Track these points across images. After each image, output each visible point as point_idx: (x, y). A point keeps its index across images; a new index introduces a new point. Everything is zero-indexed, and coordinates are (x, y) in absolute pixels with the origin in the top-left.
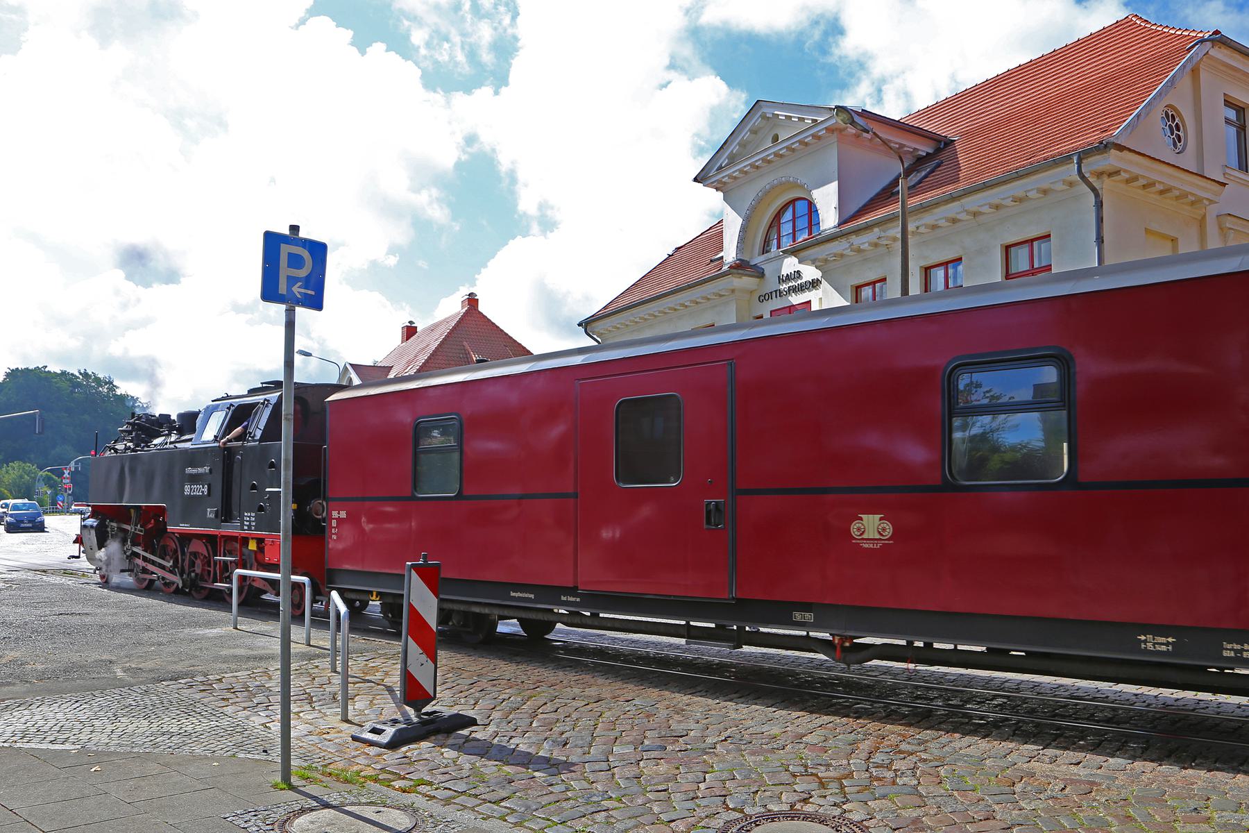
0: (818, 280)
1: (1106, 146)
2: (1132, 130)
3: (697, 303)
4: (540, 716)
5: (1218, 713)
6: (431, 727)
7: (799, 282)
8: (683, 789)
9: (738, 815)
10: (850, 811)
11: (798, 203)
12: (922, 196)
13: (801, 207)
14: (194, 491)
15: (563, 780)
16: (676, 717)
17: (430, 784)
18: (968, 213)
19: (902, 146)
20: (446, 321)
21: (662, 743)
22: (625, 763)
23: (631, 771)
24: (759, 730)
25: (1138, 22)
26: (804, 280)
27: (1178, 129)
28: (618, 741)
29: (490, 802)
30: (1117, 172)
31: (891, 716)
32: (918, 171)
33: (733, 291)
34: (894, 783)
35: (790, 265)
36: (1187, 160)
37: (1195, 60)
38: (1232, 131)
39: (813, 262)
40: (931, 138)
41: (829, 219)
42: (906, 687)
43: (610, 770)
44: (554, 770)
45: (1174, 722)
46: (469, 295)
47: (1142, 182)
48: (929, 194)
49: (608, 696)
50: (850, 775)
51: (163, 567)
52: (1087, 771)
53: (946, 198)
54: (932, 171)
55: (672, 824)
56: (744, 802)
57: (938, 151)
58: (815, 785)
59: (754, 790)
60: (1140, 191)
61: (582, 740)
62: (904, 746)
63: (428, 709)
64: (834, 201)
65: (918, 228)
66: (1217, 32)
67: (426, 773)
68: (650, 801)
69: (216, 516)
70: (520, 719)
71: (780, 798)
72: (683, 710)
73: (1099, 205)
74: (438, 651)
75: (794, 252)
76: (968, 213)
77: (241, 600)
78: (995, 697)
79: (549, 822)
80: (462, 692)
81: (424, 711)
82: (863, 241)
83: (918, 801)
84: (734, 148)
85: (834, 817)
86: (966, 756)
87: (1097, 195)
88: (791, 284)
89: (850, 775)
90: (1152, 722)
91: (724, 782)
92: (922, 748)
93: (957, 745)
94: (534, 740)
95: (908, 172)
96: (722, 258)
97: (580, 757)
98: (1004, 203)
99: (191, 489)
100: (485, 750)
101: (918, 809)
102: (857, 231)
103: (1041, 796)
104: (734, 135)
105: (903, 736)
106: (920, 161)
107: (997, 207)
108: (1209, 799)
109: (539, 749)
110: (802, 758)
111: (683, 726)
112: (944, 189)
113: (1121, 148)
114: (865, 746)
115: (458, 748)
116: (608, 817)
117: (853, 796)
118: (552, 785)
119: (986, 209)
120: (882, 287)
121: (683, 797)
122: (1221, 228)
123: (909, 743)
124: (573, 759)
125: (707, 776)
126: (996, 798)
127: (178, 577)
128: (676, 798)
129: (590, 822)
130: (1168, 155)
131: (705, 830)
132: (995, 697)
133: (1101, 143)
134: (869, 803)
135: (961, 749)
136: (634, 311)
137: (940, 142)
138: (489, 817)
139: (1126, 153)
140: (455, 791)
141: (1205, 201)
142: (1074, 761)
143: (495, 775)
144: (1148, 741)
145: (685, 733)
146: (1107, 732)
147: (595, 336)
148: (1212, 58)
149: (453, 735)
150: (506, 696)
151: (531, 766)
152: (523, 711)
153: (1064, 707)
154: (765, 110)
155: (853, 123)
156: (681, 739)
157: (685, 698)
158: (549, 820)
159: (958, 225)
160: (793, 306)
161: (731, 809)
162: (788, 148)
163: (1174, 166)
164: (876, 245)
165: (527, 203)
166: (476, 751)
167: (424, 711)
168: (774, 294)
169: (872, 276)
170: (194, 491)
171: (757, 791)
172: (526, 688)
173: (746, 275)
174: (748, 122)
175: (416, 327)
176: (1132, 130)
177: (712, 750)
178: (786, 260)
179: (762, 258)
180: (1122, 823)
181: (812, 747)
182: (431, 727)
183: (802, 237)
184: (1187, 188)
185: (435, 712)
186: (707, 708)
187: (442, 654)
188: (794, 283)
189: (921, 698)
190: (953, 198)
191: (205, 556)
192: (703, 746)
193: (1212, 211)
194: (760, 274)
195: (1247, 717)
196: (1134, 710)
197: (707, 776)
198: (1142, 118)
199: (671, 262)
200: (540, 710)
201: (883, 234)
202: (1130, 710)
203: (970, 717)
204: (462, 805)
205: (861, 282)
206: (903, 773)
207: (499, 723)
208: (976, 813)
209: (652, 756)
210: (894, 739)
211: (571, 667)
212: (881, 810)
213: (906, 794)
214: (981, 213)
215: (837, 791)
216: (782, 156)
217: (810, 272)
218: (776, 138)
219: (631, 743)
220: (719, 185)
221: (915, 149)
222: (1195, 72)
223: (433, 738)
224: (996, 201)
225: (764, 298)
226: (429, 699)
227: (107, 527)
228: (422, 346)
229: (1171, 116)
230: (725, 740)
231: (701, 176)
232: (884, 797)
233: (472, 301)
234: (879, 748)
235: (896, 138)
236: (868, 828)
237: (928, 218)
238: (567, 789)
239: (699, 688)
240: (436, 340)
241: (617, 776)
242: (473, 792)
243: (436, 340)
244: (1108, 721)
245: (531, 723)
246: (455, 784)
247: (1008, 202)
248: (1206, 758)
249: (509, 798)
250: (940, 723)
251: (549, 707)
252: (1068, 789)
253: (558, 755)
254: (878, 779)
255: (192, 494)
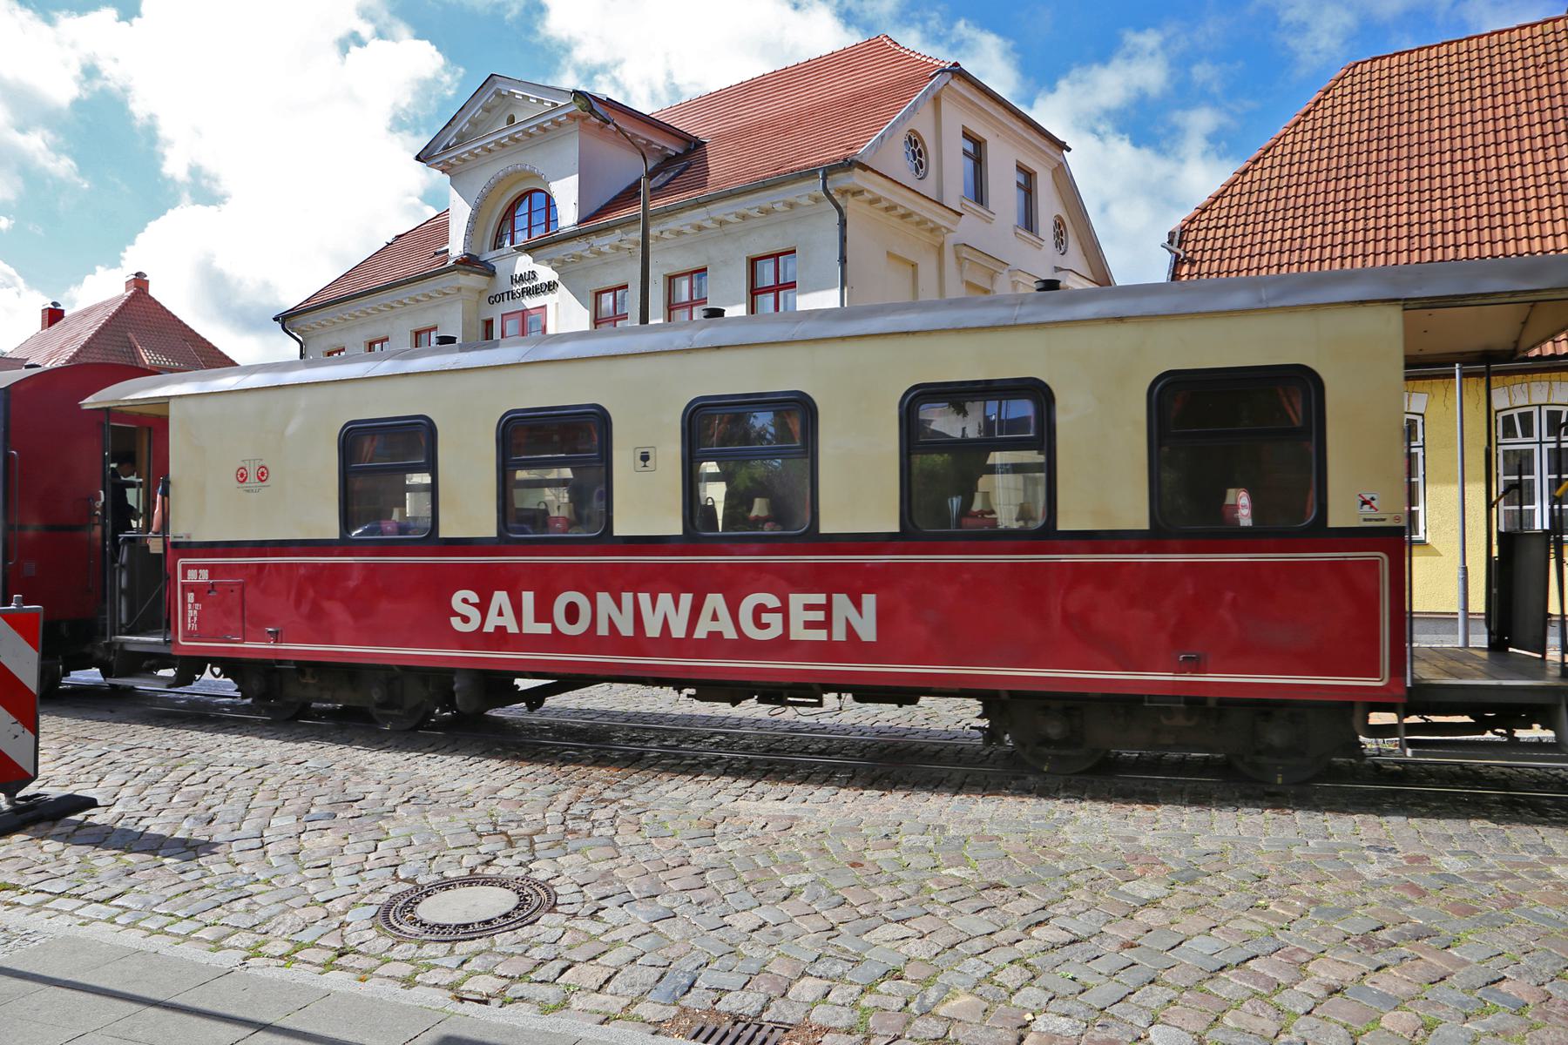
0: (554, 282)
1: (850, 164)
2: (875, 152)
3: (417, 301)
4: (184, 790)
5: (926, 738)
6: (30, 814)
7: (534, 283)
8: (348, 862)
9: (408, 886)
10: (537, 870)
11: (536, 196)
12: (668, 199)
13: (539, 200)
15: (200, 865)
16: (355, 779)
17: (16, 887)
18: (714, 221)
19: (650, 142)
20: (104, 305)
21: (332, 810)
22: (282, 837)
23: (292, 845)
24: (450, 787)
25: (888, 43)
26: (539, 282)
27: (921, 156)
28: (278, 812)
29: (97, 902)
30: (861, 192)
31: (600, 761)
32: (666, 172)
33: (459, 289)
34: (589, 835)
35: (524, 264)
36: (928, 188)
37: (937, 88)
38: (970, 163)
39: (549, 262)
40: (680, 138)
41: (567, 216)
42: (622, 728)
43: (262, 847)
44: (191, 853)
45: (882, 750)
46: (136, 275)
47: (884, 204)
48: (675, 198)
49: (275, 759)
50: (543, 831)
52: (792, 806)
53: (692, 203)
54: (680, 173)
55: (328, 905)
56: (418, 871)
57: (688, 152)
58: (502, 845)
59: (431, 856)
60: (883, 213)
61: (233, 814)
62: (608, 794)
63: (30, 790)
64: (574, 196)
65: (662, 232)
66: (956, 64)
67: (12, 874)
68: (305, 880)
70: (157, 796)
71: (460, 863)
72: (364, 770)
73: (843, 224)
74: (42, 718)
75: (528, 249)
76: (714, 221)
77: (40, 651)
78: (713, 735)
79: (173, 919)
80: (83, 767)
81: (18, 796)
82: (604, 242)
83: (611, 852)
84: (463, 125)
85: (518, 879)
86: (672, 799)
87: (841, 213)
88: (524, 286)
89: (543, 831)
90: (862, 751)
91: (398, 850)
92: (627, 794)
93: (664, 788)
94: (170, 819)
95: (651, 175)
96: (447, 251)
97: (226, 834)
98: (750, 213)
100: (104, 838)
101: (610, 861)
102: (598, 232)
103: (741, 836)
104: (464, 110)
105: (608, 782)
106: (668, 161)
107: (744, 217)
108: (901, 823)
109: (176, 829)
110: (492, 815)
111: (362, 788)
112: (691, 193)
113: (865, 168)
114: (564, 798)
115: (67, 838)
116: (250, 904)
117: (542, 853)
118: (185, 872)
119: (732, 218)
120: (623, 296)
121: (348, 871)
122: (957, 258)
123: (613, 790)
124: (217, 838)
125: (380, 844)
126: (694, 842)
128: (338, 873)
129: (225, 913)
130: (908, 178)
131: (366, 907)
132: (713, 735)
133: (845, 160)
134: (558, 860)
135: (667, 792)
136: (342, 306)
137: (691, 142)
138: (92, 921)
139: (869, 173)
140: (50, 893)
141: (943, 230)
142: (780, 797)
143: (111, 867)
144: (854, 771)
145: (362, 796)
146: (817, 764)
147: (295, 334)
148: (952, 88)
149: (62, 822)
150: (143, 768)
151: (161, 852)
152: (162, 785)
153: (782, 740)
154: (499, 86)
155: (592, 111)
156: (355, 804)
157: (369, 756)
158: (172, 915)
159: (704, 232)
160: (527, 310)
161: (402, 880)
162: (524, 132)
163: (914, 191)
164: (618, 248)
165: (175, 166)
166: (91, 839)
167: (18, 796)
168: (506, 295)
169: (614, 283)
171: (435, 857)
172: (172, 755)
173: (474, 272)
174: (482, 97)
175: (63, 311)
176: (875, 152)
177: (390, 814)
178: (520, 258)
179: (494, 254)
180: (815, 857)
181: (506, 802)
182: (30, 814)
183: (538, 233)
184: (928, 215)
185: (38, 795)
186: (393, 766)
187: (47, 723)
188: (528, 285)
189: (635, 741)
190: (699, 204)
192: (380, 810)
193: (950, 240)
194: (490, 271)
196: (847, 739)
197: (380, 844)
198: (886, 138)
199: (388, 251)
200: (186, 782)
201: (625, 237)
202: (844, 740)
203: (683, 758)
204: (56, 910)
205: (602, 287)
206: (601, 824)
207: (129, 801)
208: (671, 860)
209: (317, 827)
210: (598, 786)
211: (234, 727)
212: (570, 866)
213: (600, 846)
214: (728, 223)
215: (526, 849)
216: (517, 140)
217: (546, 274)
218: (511, 120)
219: (295, 812)
220: (446, 167)
221: (663, 147)
222: (937, 100)
223: (32, 828)
224: (742, 210)
225: (495, 299)
226: (29, 779)
228: (68, 335)
229: (915, 143)
230: (408, 801)
231: (424, 154)
232: (576, 851)
233: (140, 283)
234: (580, 798)
235: (644, 134)
236: (552, 887)
237: (673, 224)
238: (204, 876)
239: (388, 744)
240: (91, 328)
241: (269, 854)
242: (75, 891)
243: (91, 328)
244: (821, 752)
245: (171, 799)
246: (52, 884)
247: (754, 213)
248: (906, 783)
249: (123, 894)
250: (651, 766)
251: (199, 777)
252: (768, 827)
253: (200, 834)
254: (574, 832)
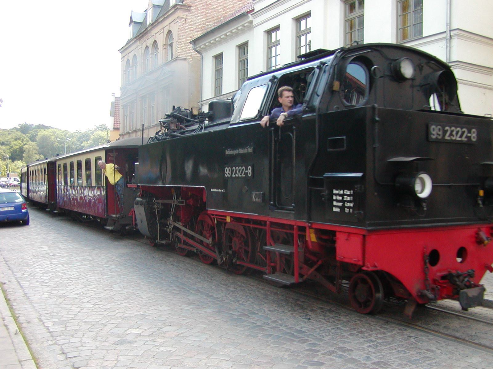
14: (236, 173)
51: (202, 243)
69: (264, 200)
99: (232, 171)
127: (217, 254)
170: (236, 173)
191: (242, 236)
195: (492, 315)
227: (154, 204)
255: (233, 176)
